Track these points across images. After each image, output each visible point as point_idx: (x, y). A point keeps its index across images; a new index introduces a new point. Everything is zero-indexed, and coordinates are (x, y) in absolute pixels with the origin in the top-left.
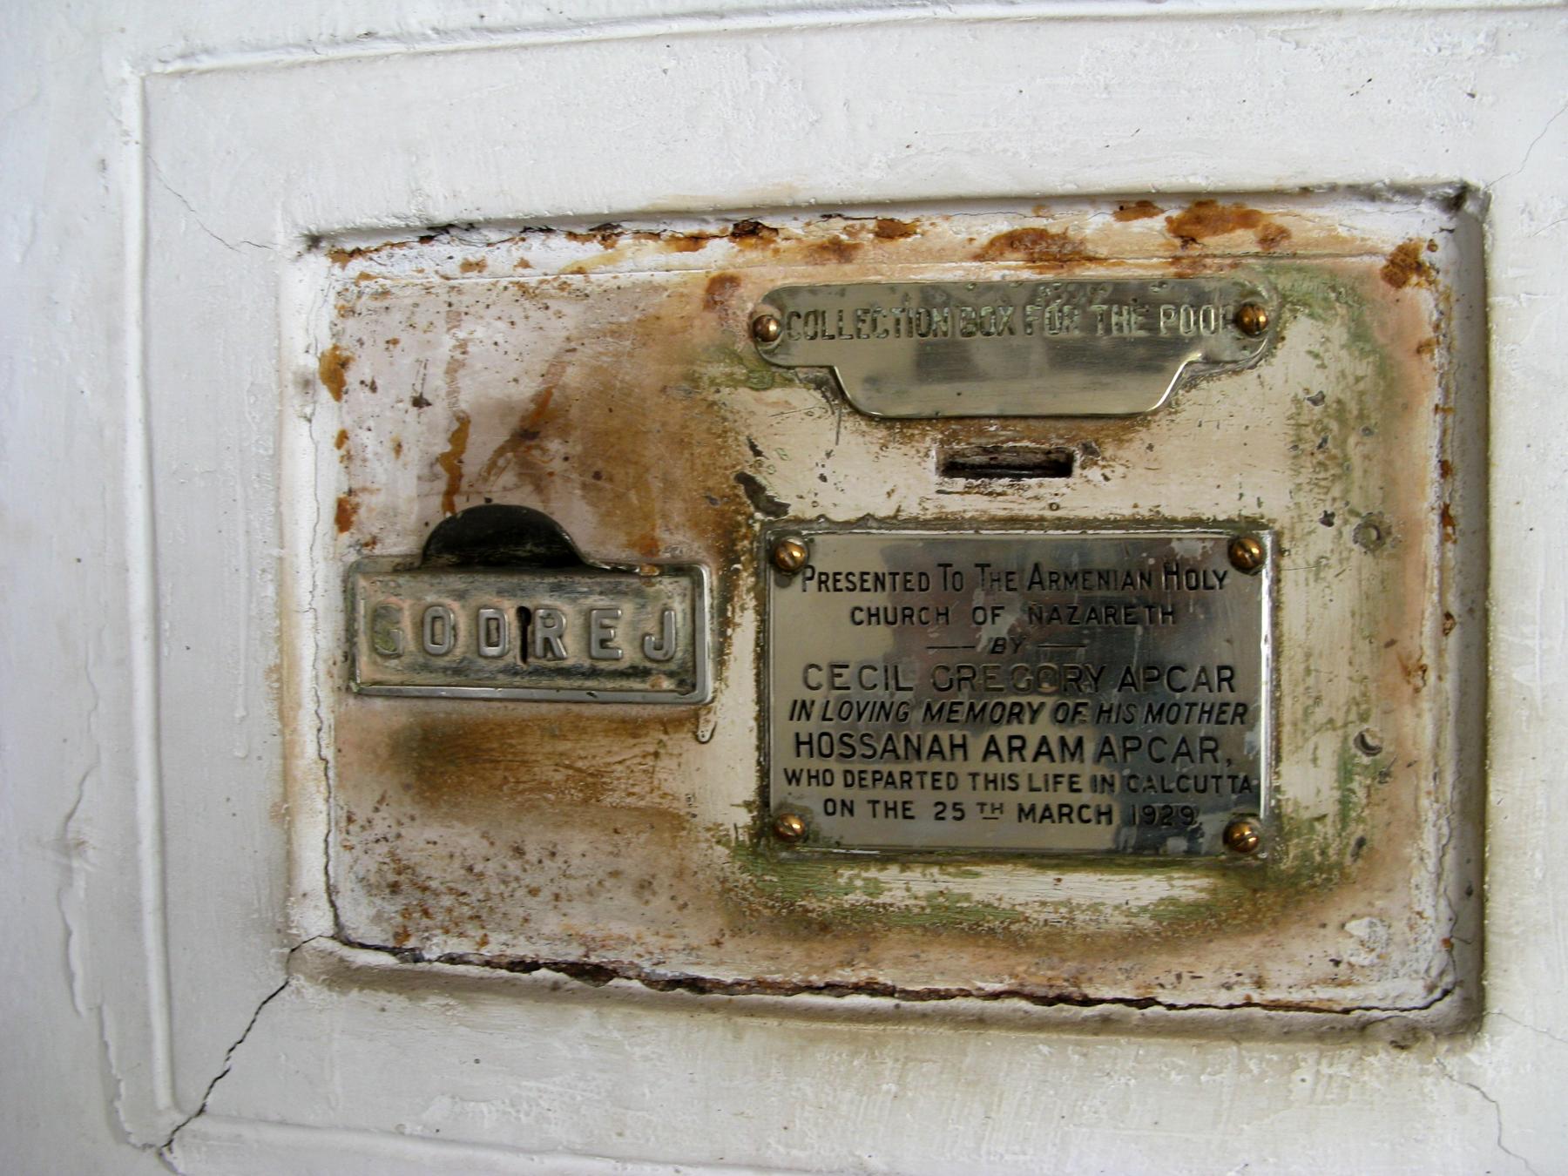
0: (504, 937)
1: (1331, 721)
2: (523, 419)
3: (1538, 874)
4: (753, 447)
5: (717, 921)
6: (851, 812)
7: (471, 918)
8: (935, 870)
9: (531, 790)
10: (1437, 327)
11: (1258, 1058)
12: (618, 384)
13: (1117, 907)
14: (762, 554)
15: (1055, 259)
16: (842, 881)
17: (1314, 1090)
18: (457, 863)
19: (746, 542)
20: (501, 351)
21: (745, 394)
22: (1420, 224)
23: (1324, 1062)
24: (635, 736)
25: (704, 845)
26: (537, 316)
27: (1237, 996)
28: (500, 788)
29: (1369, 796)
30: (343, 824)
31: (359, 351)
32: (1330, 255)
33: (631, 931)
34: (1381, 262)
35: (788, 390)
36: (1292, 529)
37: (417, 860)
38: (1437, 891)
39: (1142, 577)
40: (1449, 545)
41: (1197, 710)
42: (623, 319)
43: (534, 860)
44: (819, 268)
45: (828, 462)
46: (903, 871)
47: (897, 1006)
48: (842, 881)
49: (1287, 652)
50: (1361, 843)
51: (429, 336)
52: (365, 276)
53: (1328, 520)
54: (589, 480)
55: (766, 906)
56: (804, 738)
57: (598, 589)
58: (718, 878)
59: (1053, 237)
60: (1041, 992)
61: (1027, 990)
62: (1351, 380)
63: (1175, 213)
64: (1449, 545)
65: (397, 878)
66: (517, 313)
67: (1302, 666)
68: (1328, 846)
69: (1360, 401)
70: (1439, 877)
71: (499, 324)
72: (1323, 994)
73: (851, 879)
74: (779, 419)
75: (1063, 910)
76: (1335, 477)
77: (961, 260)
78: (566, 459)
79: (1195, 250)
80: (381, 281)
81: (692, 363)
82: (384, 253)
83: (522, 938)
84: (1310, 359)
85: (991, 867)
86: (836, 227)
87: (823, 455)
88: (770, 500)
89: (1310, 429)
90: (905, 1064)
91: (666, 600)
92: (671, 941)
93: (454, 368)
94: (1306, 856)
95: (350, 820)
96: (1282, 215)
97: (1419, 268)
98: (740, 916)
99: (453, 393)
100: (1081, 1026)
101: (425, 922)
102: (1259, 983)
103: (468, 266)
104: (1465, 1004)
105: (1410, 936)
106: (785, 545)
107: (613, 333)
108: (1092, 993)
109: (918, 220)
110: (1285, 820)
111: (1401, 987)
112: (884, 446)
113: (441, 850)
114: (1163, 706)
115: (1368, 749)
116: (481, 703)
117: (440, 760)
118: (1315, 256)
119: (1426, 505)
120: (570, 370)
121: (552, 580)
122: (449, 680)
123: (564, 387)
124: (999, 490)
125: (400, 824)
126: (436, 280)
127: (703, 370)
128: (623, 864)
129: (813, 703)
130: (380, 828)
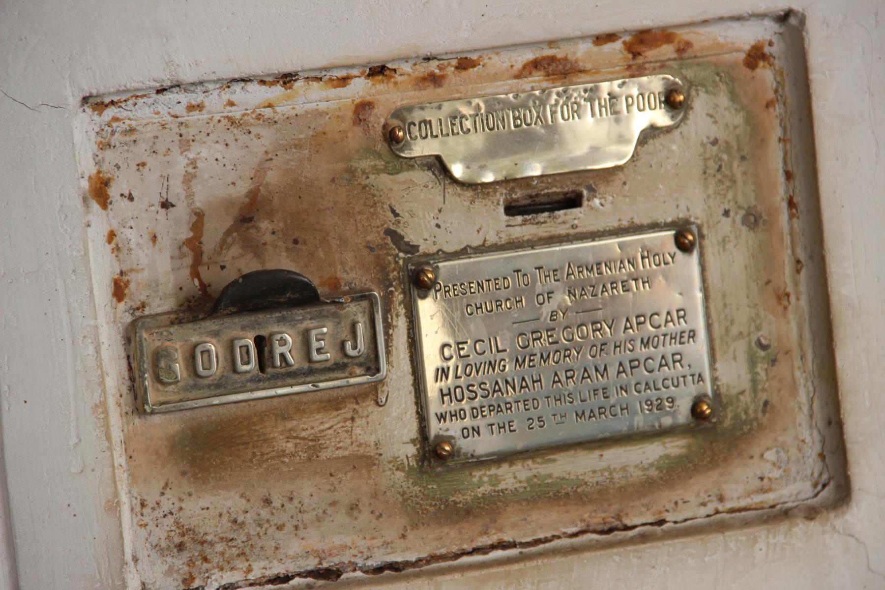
0: (263, 564)
1: (741, 333)
2: (241, 209)
3: (868, 404)
4: (393, 211)
5: (401, 521)
6: (479, 433)
7: (238, 555)
8: (530, 462)
9: (273, 458)
10: (776, 91)
11: (735, 539)
12: (304, 180)
13: (636, 466)
14: (406, 279)
15: (561, 73)
16: (475, 480)
17: (767, 555)
18: (225, 517)
19: (395, 273)
20: (221, 165)
21: (385, 178)
22: (762, 32)
23: (771, 536)
24: (337, 409)
25: (389, 473)
26: (243, 138)
27: (710, 509)
28: (251, 460)
29: (767, 374)
30: (138, 509)
31: (117, 173)
32: (716, 55)
33: (348, 540)
34: (742, 56)
35: (411, 173)
36: (708, 222)
37: (196, 523)
38: (811, 426)
39: (629, 262)
40: (795, 220)
41: (668, 338)
42: (302, 136)
43: (279, 506)
44: (423, 92)
45: (440, 216)
46: (511, 466)
47: (521, 553)
48: (475, 480)
49: (712, 295)
50: (766, 403)
51: (168, 158)
52: (115, 119)
53: (726, 213)
54: (291, 245)
55: (431, 505)
56: (445, 391)
57: (309, 316)
58: (399, 493)
59: (559, 60)
60: (600, 528)
61: (591, 528)
62: (731, 128)
63: (628, 38)
64: (795, 220)
65: (182, 539)
66: (230, 138)
67: (722, 303)
68: (748, 409)
69: (738, 140)
70: (811, 416)
71: (217, 145)
72: (757, 499)
73: (480, 477)
74: (407, 191)
75: (606, 474)
76: (728, 188)
77: (507, 79)
78: (274, 233)
79: (640, 60)
80: (127, 122)
81: (350, 160)
82: (130, 103)
83: (275, 562)
84: (708, 118)
85: (562, 454)
86: (433, 66)
87: (436, 211)
88: (408, 244)
89: (712, 161)
90: (538, 585)
91: (352, 317)
92: (374, 542)
93: (188, 179)
94: (736, 417)
95: (143, 505)
96: (687, 33)
97: (763, 57)
98: (418, 514)
99: (190, 196)
100: (632, 541)
101: (206, 566)
102: (721, 499)
103: (191, 108)
104: (837, 485)
105: (800, 455)
106: (423, 272)
107: (296, 146)
108: (629, 522)
109: (481, 57)
110: (723, 397)
111: (796, 489)
112: (472, 202)
113: (213, 513)
114: (649, 339)
115: (764, 347)
116: (232, 406)
117: (207, 450)
118: (706, 56)
119: (779, 198)
120: (270, 173)
121: (277, 315)
122: (213, 393)
123: (267, 184)
124: (542, 220)
125: (181, 500)
126: (169, 119)
127: (357, 165)
128: (337, 496)
129: (448, 368)
130: (166, 506)
